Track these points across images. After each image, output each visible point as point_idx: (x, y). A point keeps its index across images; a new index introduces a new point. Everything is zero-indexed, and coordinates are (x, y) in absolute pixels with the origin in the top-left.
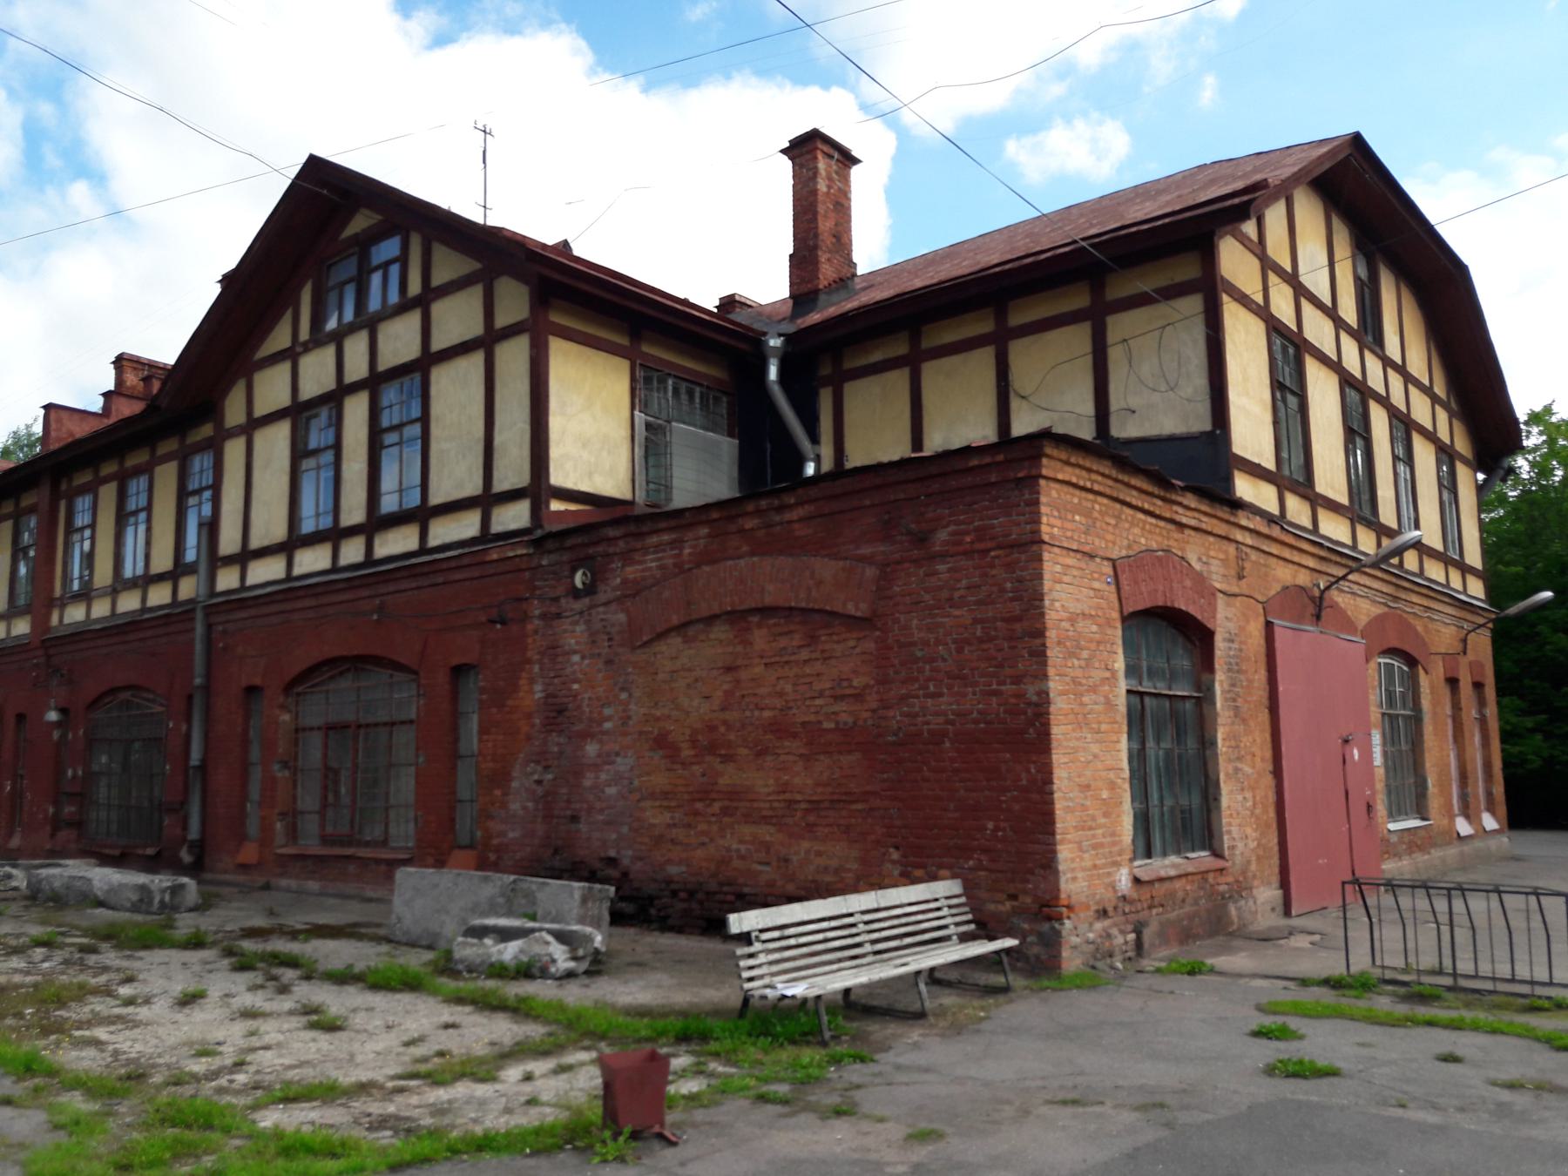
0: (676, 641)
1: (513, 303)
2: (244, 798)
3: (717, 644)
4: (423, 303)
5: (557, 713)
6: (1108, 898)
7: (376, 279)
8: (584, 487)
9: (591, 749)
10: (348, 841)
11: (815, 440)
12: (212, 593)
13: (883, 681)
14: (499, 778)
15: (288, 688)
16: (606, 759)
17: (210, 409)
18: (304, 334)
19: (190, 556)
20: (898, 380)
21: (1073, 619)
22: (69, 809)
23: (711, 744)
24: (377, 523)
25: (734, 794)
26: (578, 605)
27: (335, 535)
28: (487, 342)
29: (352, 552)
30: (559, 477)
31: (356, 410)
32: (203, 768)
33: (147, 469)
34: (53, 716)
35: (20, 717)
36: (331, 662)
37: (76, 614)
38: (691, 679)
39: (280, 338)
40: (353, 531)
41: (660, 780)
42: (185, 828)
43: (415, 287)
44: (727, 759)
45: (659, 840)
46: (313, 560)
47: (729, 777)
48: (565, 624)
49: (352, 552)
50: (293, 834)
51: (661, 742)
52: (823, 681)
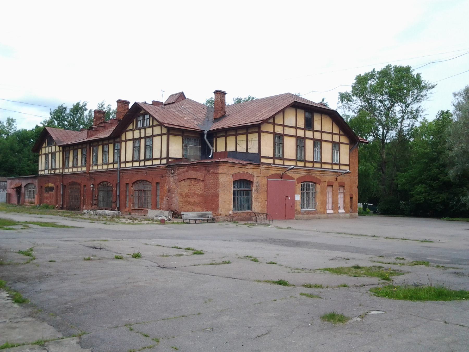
0: (183, 181)
1: (165, 131)
2: (126, 201)
3: (188, 182)
4: (153, 127)
5: (169, 190)
6: (228, 214)
7: (146, 120)
8: (175, 157)
9: (173, 195)
10: (142, 207)
11: (213, 147)
12: (120, 168)
13: (205, 188)
14: (162, 199)
15: (133, 184)
16: (175, 197)
17: (119, 136)
18: (134, 128)
19: (116, 161)
20: (224, 138)
21: (224, 182)
22: (95, 202)
23: (187, 195)
24: (145, 160)
25: (189, 202)
26: (172, 175)
27: (140, 161)
28: (161, 135)
29: (142, 164)
30: (171, 156)
31: (143, 141)
32: (119, 195)
33: (108, 144)
34: (92, 186)
35: (85, 186)
36: (140, 180)
37: (95, 168)
38: (185, 187)
39: (130, 127)
40: (142, 160)
41: (181, 200)
42: (116, 205)
43: (151, 124)
44: (189, 197)
45: (181, 208)
46: (136, 164)
47: (189, 199)
48: (170, 178)
49: (142, 164)
50: (134, 206)
51: (181, 195)
52: (198, 188)
